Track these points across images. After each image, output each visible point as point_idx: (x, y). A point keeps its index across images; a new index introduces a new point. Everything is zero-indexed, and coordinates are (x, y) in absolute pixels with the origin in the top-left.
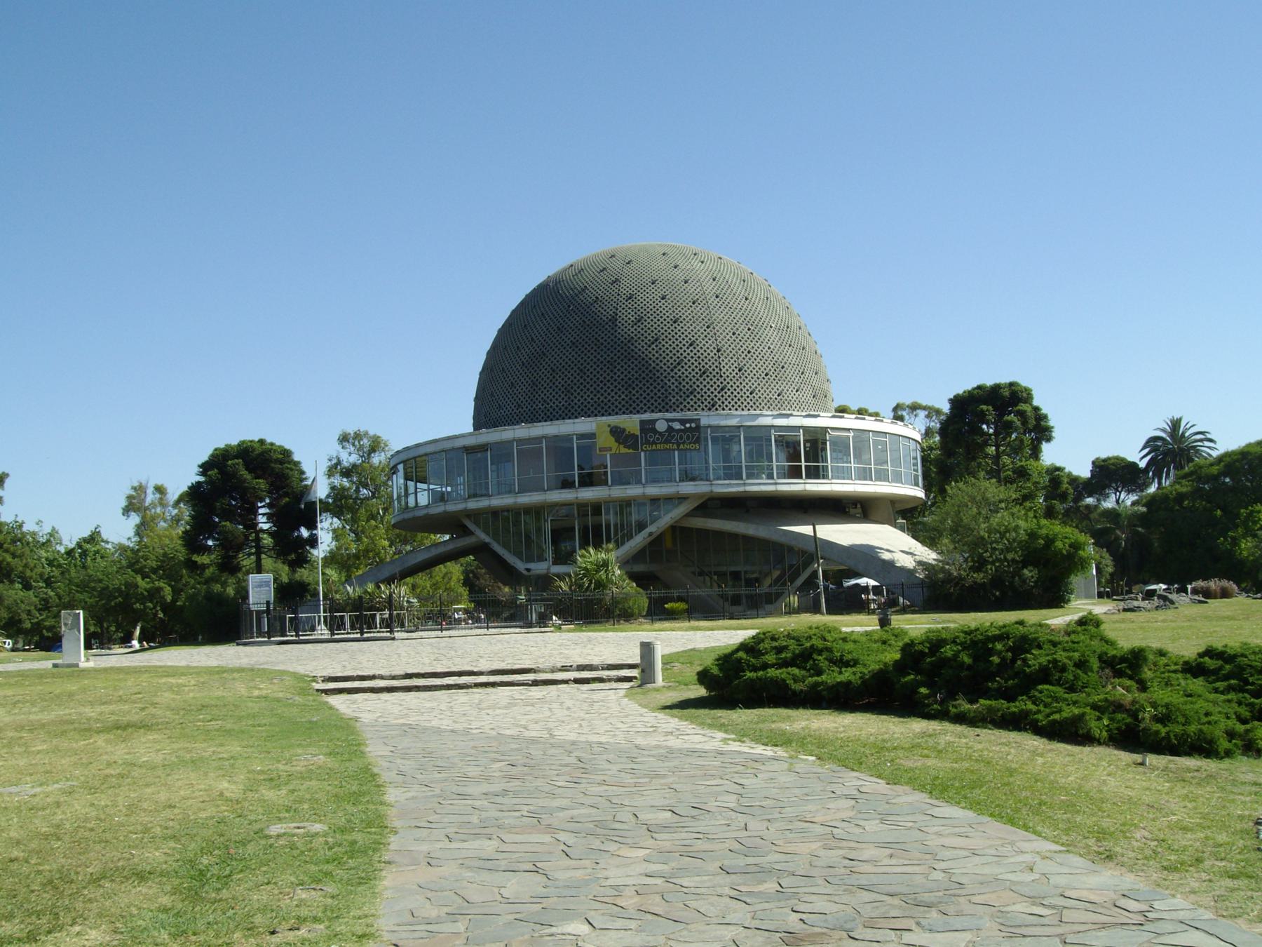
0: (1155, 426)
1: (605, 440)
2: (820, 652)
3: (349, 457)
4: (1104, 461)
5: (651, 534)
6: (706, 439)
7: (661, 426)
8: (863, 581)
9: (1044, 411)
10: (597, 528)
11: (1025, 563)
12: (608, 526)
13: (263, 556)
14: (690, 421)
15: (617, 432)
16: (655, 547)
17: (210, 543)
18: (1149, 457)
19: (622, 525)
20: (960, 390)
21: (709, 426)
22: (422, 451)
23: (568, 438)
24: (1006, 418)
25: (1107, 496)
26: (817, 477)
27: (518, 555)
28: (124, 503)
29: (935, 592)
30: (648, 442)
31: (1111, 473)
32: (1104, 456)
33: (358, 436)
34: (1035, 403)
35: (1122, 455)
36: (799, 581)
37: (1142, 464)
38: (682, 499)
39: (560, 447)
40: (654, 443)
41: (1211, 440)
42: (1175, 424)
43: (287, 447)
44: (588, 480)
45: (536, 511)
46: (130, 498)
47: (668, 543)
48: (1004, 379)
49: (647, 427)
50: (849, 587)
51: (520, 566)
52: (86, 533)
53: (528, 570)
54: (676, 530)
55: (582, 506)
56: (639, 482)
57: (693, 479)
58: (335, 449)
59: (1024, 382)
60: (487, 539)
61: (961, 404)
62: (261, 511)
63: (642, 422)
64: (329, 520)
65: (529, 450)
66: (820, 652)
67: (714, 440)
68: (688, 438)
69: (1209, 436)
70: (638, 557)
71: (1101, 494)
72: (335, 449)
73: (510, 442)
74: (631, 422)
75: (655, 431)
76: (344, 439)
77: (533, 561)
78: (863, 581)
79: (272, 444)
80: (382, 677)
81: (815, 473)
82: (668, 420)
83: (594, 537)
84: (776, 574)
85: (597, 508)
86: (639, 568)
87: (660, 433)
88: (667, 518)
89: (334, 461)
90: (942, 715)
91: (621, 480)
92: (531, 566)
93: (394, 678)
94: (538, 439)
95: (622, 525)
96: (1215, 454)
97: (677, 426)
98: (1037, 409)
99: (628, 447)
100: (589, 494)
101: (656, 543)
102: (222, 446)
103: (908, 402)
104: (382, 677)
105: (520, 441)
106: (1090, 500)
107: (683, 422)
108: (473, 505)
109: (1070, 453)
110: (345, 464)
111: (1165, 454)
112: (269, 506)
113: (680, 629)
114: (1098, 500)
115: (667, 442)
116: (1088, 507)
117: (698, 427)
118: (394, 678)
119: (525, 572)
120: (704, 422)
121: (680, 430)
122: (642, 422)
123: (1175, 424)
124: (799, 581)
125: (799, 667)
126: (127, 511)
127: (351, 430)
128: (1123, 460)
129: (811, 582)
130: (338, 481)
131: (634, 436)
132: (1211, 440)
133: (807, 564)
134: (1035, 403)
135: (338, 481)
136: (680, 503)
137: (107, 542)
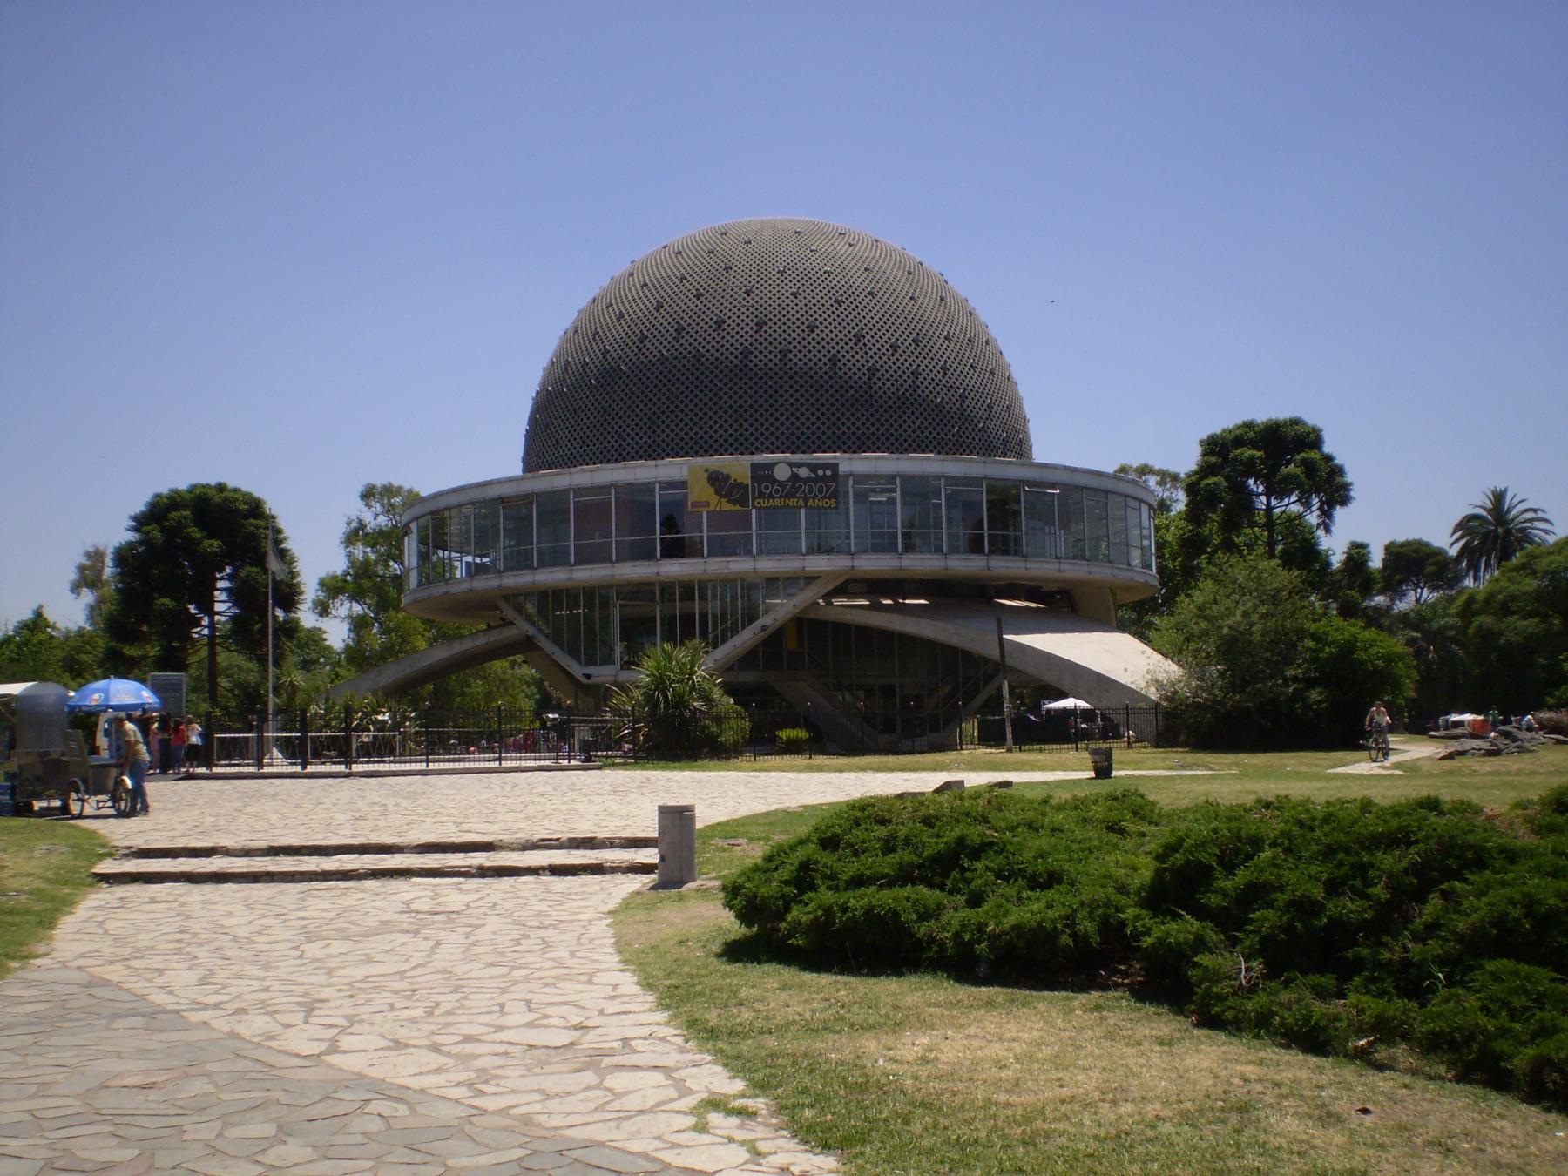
0: (1473, 501)
1: (701, 492)
2: (978, 852)
3: (374, 518)
4: (1402, 545)
5: (764, 628)
6: (847, 494)
7: (782, 473)
8: (1069, 703)
9: (1338, 461)
10: (688, 619)
11: (1310, 683)
12: (704, 617)
13: (218, 649)
14: (825, 466)
15: (718, 480)
16: (771, 649)
17: (145, 628)
18: (1462, 543)
19: (724, 615)
20: (1217, 429)
21: (851, 474)
22: (442, 503)
23: (647, 488)
24: (1284, 470)
25: (1403, 594)
26: (1006, 552)
27: (573, 652)
28: (72, 575)
29: (1179, 726)
30: (761, 495)
31: (1410, 561)
32: (1401, 538)
33: (389, 491)
34: (1327, 449)
35: (1426, 539)
36: (979, 701)
37: (1453, 552)
38: (811, 579)
39: (635, 500)
40: (771, 496)
41: (1546, 521)
42: (1499, 497)
43: (257, 494)
44: (675, 549)
45: (595, 596)
46: (82, 569)
47: (791, 643)
48: (1281, 413)
49: (762, 474)
50: (1049, 711)
51: (577, 670)
52: (27, 615)
53: (588, 677)
54: (806, 626)
55: (667, 588)
56: (749, 553)
57: (829, 551)
58: (357, 509)
59: (1311, 419)
60: (531, 631)
61: (1218, 449)
62: (220, 584)
63: (754, 467)
64: (347, 605)
65: (592, 508)
66: (978, 852)
67: (861, 497)
68: (820, 491)
69: (1540, 514)
70: (748, 659)
71: (1395, 591)
72: (357, 509)
73: (566, 492)
74: (738, 465)
75: (773, 480)
76: (368, 495)
77: (594, 663)
78: (1069, 703)
79: (236, 490)
80: (227, 852)
81: (1005, 546)
82: (791, 465)
83: (682, 629)
84: (945, 689)
85: (687, 589)
86: (748, 677)
87: (780, 483)
88: (780, 609)
89: (354, 525)
90: (1260, 1026)
91: (723, 548)
92: (589, 670)
93: (247, 853)
94: (604, 489)
95: (724, 615)
96: (1551, 539)
97: (804, 473)
98: (1329, 459)
99: (734, 502)
100: (675, 569)
101: (774, 639)
102: (164, 490)
103: (1135, 463)
104: (227, 852)
105: (579, 491)
106: (1380, 600)
107: (813, 467)
108: (512, 580)
109: (1361, 528)
110: (369, 529)
111: (1485, 537)
112: (231, 578)
113: (791, 769)
114: (1392, 600)
115: (789, 495)
116: (1377, 609)
117: (835, 475)
118: (247, 853)
119: (583, 680)
120: (844, 467)
121: (808, 479)
122: (754, 467)
123: (1499, 497)
124: (979, 701)
125: (931, 885)
126: (76, 588)
127: (379, 481)
128: (1427, 545)
129: (995, 704)
130: (359, 551)
131: (741, 486)
132: (1546, 521)
133: (988, 678)
134: (1327, 449)
135: (359, 551)
136: (807, 585)
137: (54, 628)
